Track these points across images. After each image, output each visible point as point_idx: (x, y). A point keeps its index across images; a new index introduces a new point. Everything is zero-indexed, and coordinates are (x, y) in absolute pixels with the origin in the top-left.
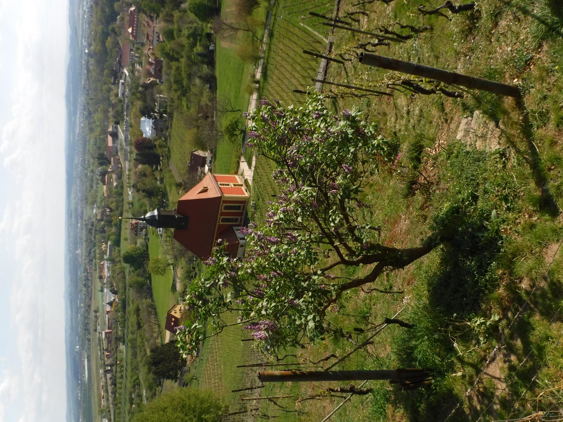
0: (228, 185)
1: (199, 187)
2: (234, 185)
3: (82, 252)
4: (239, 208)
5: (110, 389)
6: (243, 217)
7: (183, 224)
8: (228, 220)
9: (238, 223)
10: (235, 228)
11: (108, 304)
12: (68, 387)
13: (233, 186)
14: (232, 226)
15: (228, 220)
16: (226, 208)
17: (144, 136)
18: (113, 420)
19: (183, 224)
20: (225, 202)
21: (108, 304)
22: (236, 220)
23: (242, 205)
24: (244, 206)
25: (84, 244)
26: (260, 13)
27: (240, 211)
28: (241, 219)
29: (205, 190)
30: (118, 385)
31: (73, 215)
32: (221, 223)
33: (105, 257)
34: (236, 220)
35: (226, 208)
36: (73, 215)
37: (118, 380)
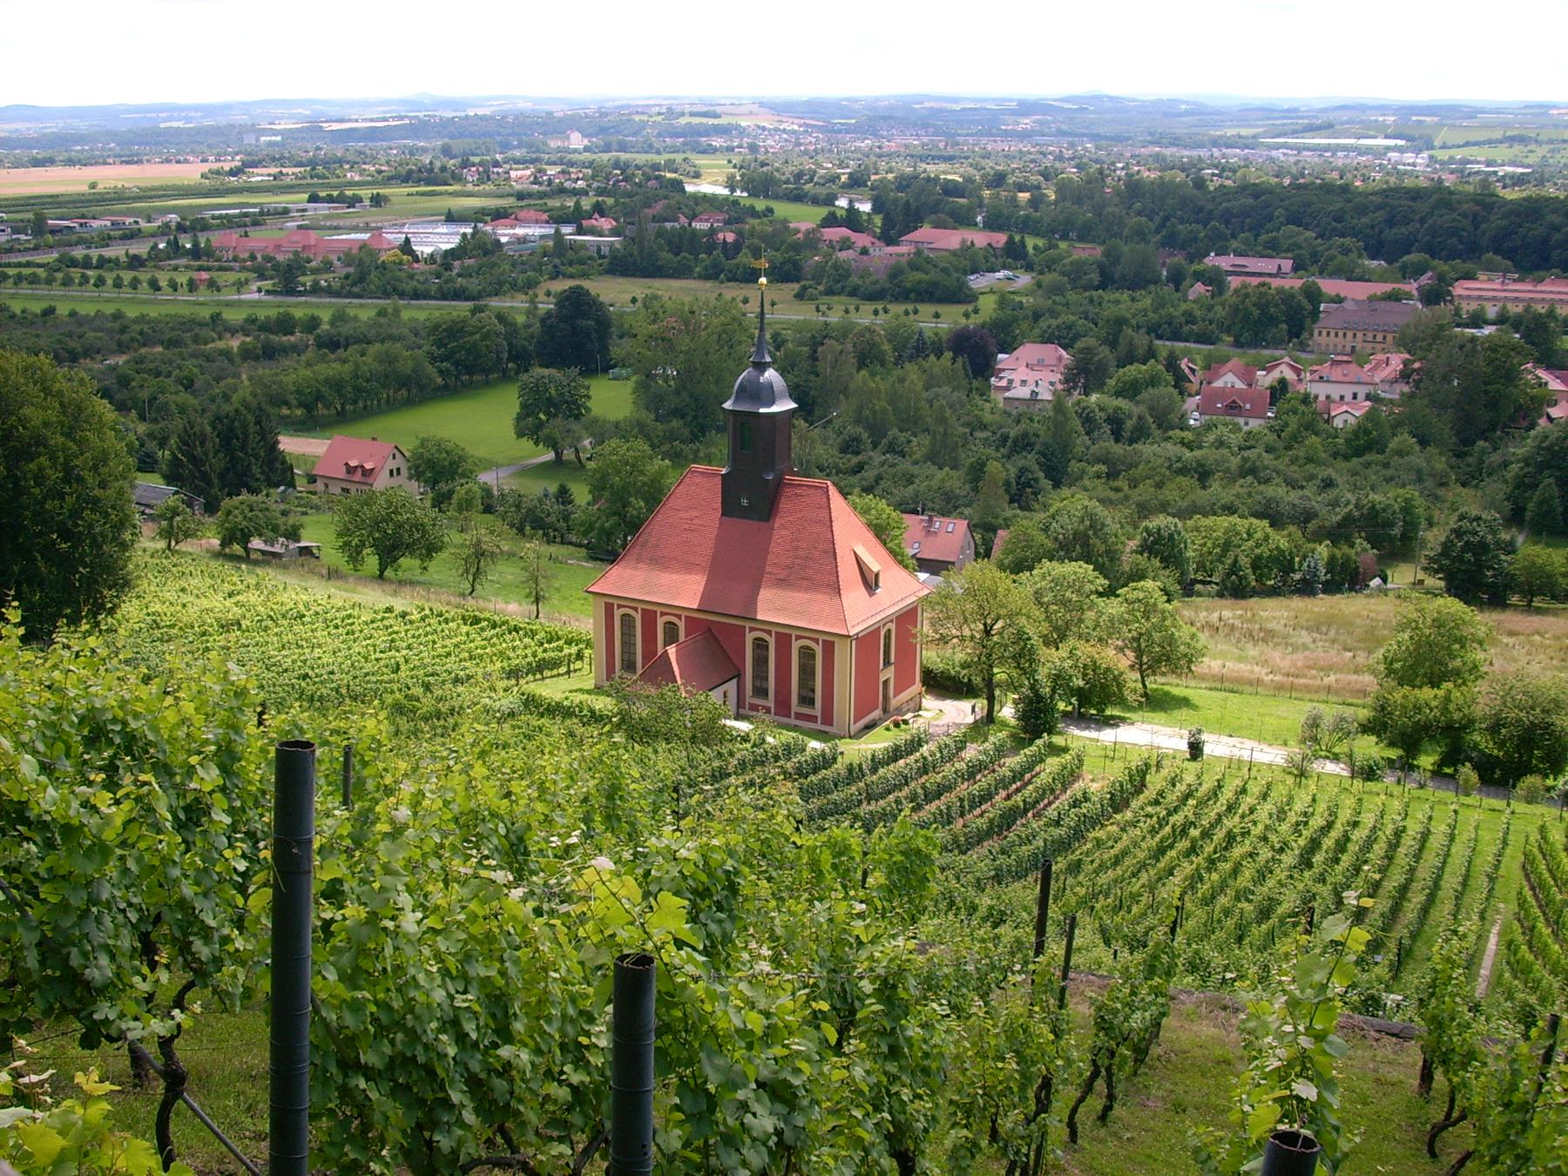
0: (887, 663)
1: (875, 560)
2: (886, 683)
3: (575, 151)
4: (807, 700)
5: (116, 251)
7: (745, 502)
8: (761, 662)
10: (731, 686)
11: (407, 241)
12: (112, 112)
13: (882, 679)
14: (739, 676)
15: (761, 662)
17: (1000, 356)
18: (5, 260)
19: (745, 502)
21: (407, 241)
23: (618, 613)
25: (605, 157)
26: (11, 272)
29: (870, 583)
30: (127, 276)
31: (711, 121)
32: (749, 638)
33: (567, 230)
34: (761, 692)
36: (711, 121)
37: (144, 276)
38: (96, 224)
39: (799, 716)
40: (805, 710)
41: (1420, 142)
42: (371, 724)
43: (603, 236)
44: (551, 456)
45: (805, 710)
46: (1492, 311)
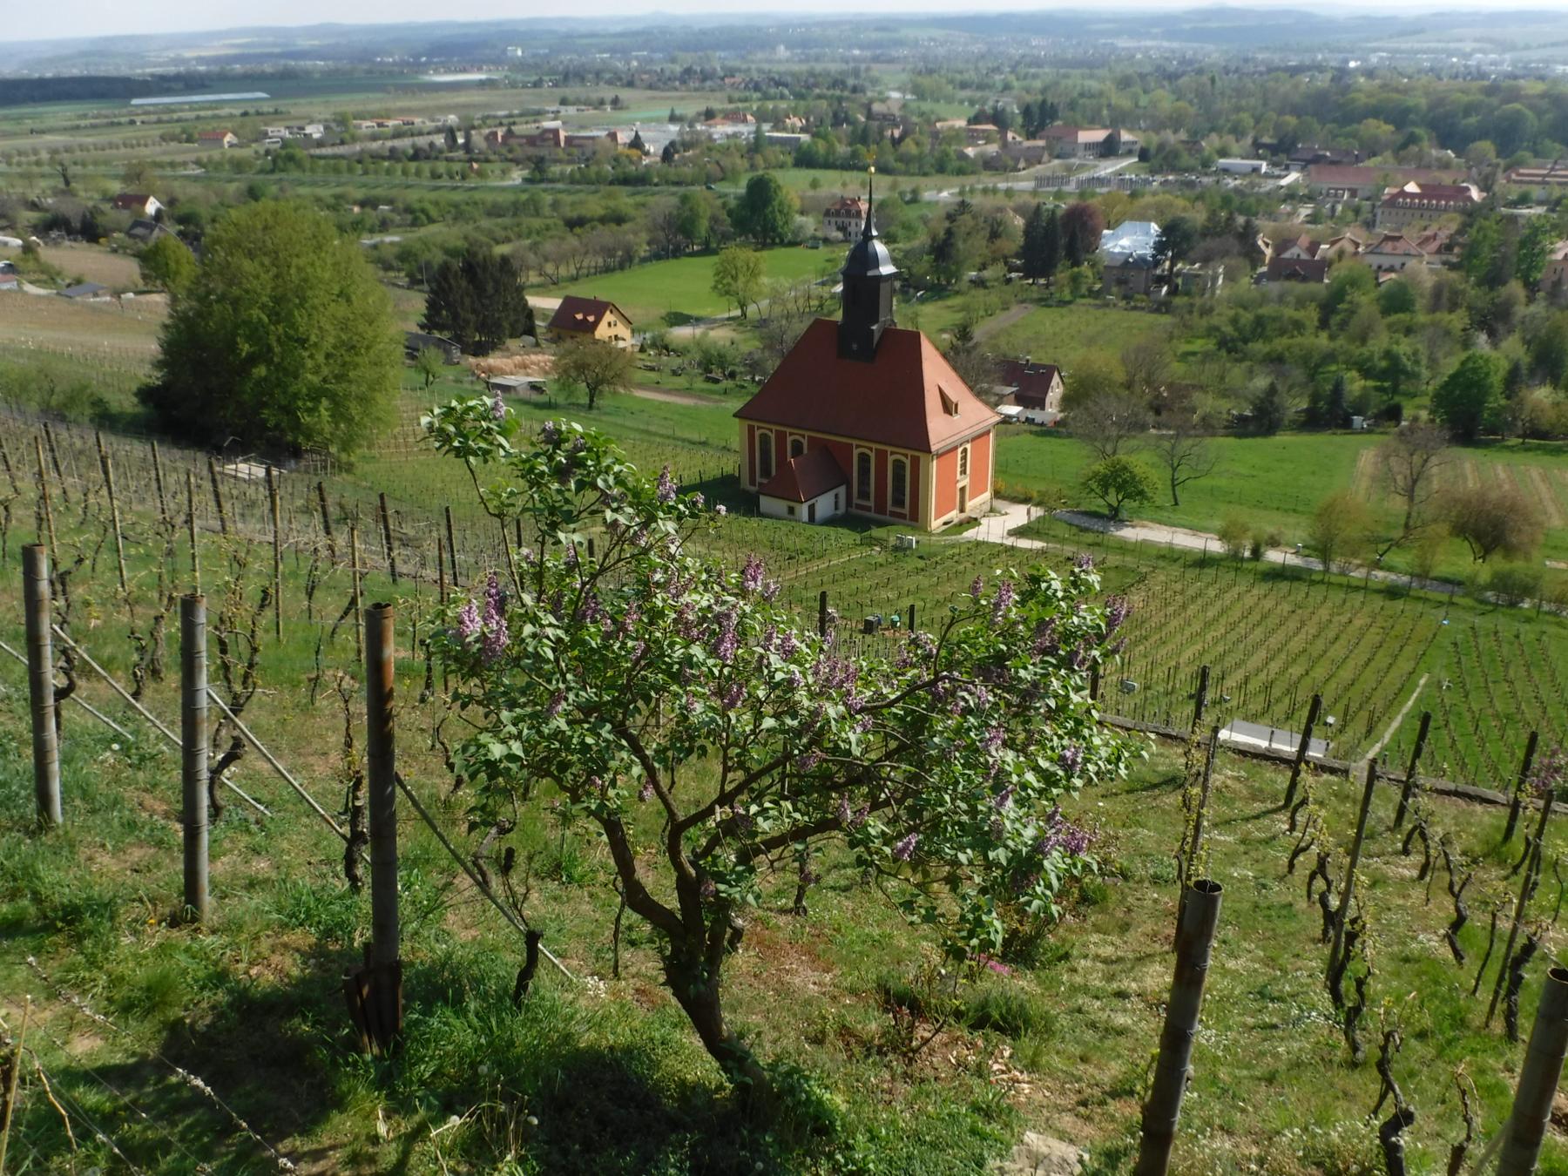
0: (964, 472)
1: (957, 390)
2: (963, 489)
3: (780, 61)
4: (899, 502)
6: (872, 515)
7: (855, 346)
8: (864, 471)
9: (856, 501)
10: (842, 490)
13: (960, 485)
15: (864, 471)
16: (899, 466)
17: (1106, 232)
20: (916, 463)
21: (637, 136)
22: (864, 495)
23: (906, 511)
24: (903, 516)
27: (890, 507)
28: (868, 509)
30: (413, 166)
32: (856, 452)
33: (766, 127)
34: (864, 495)
35: (899, 466)
38: (391, 123)
39: (893, 514)
40: (899, 510)
41: (1171, 34)
42: (1526, 606)
43: (795, 130)
44: (738, 312)
45: (899, 510)
46: (1537, 192)
